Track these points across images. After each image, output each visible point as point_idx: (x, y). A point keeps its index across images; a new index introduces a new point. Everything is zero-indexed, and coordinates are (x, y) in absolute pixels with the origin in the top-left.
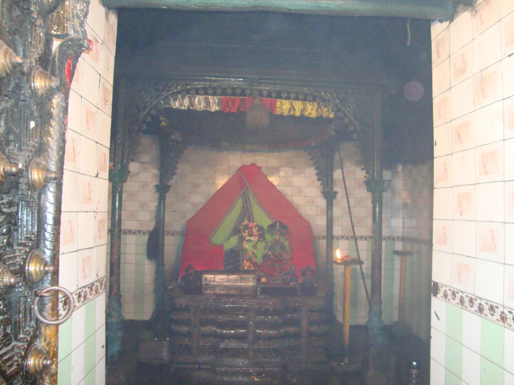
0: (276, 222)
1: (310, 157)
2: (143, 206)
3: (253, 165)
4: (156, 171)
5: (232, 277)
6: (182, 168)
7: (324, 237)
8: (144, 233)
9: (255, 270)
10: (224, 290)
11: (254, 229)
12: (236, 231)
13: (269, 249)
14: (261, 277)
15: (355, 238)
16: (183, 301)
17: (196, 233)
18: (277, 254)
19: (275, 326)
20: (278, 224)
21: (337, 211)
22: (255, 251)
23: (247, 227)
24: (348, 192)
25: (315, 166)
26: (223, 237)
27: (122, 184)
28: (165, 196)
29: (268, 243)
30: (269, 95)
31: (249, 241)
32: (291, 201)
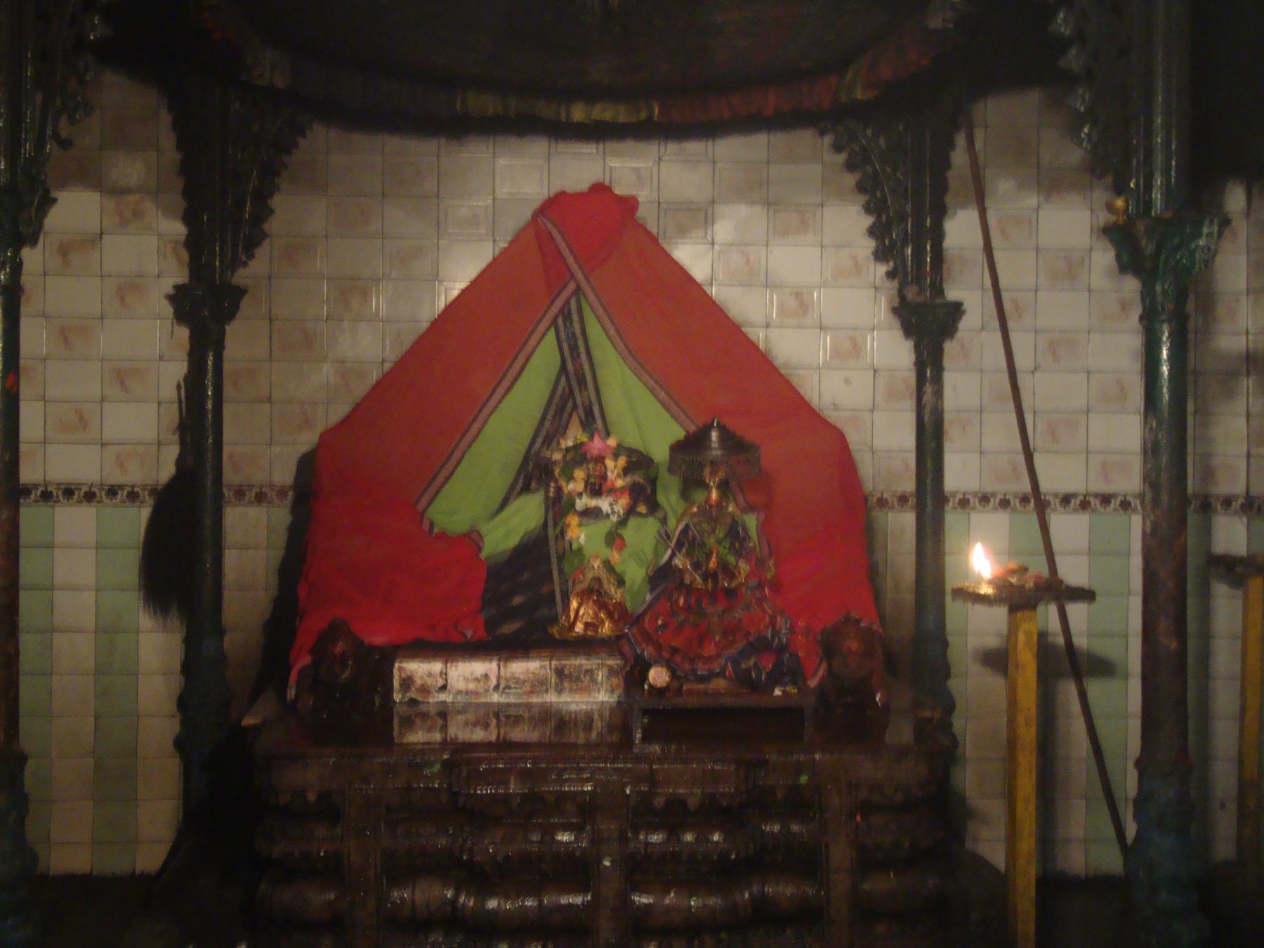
1: (842, 157)
2: (123, 377)
3: (600, 189)
4: (178, 229)
5: (521, 668)
6: (291, 212)
7: (903, 499)
8: (133, 496)
10: (486, 726)
11: (610, 463)
12: (534, 473)
13: (679, 545)
14: (648, 667)
15: (1037, 501)
16: (309, 776)
17: (362, 478)
18: (712, 564)
19: (720, 873)
20: (714, 435)
21: (962, 387)
22: (615, 557)
23: (578, 456)
24: (1008, 306)
25: (863, 199)
26: (479, 504)
27: (17, 252)
31: (591, 514)
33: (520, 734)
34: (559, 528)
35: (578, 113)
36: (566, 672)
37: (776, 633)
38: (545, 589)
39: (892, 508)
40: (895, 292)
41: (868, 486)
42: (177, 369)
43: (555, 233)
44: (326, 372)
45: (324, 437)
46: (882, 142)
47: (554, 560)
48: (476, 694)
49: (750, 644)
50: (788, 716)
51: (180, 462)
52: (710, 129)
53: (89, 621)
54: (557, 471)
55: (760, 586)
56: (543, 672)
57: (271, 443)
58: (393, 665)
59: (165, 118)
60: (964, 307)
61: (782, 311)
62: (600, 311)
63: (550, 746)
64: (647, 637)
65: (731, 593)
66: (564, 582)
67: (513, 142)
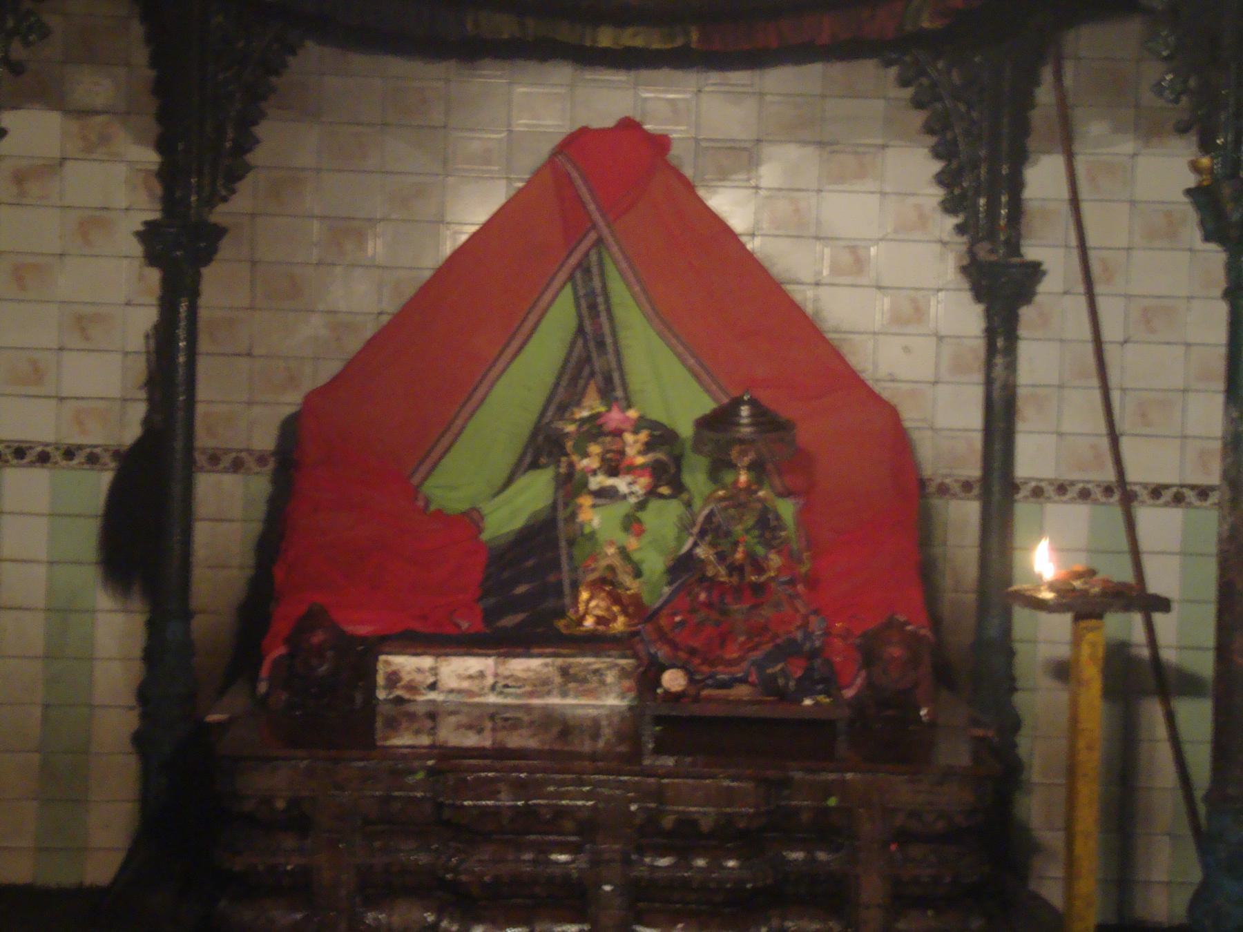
0: (737, 403)
1: (909, 92)
2: (84, 324)
3: (629, 125)
4: (150, 158)
5: (521, 666)
6: (279, 141)
7: (967, 486)
8: (93, 459)
9: (635, 634)
10: (480, 731)
11: (629, 437)
12: (544, 447)
13: (702, 533)
14: (663, 668)
15: (1123, 494)
16: (277, 782)
17: (345, 455)
18: (739, 556)
20: (745, 411)
21: (1039, 360)
22: (632, 543)
23: (594, 429)
26: (482, 481)
28: (197, 279)
29: (698, 503)
32: (809, 309)
33: (515, 741)
34: (569, 510)
35: (605, 38)
36: (572, 671)
37: (808, 636)
38: (552, 578)
39: (954, 496)
40: (964, 248)
41: (927, 472)
42: (148, 316)
43: (575, 175)
44: (315, 326)
45: (309, 398)
46: (956, 77)
47: (563, 544)
48: (470, 693)
49: (777, 646)
50: (816, 726)
51: (147, 422)
52: (755, 59)
53: (38, 597)
54: (569, 445)
55: (792, 582)
56: (546, 670)
57: (250, 403)
58: (377, 660)
59: (137, 29)
60: (1044, 267)
61: (836, 269)
62: (624, 265)
63: (552, 754)
64: (662, 636)
65: (758, 588)
66: (574, 569)
67: (532, 67)
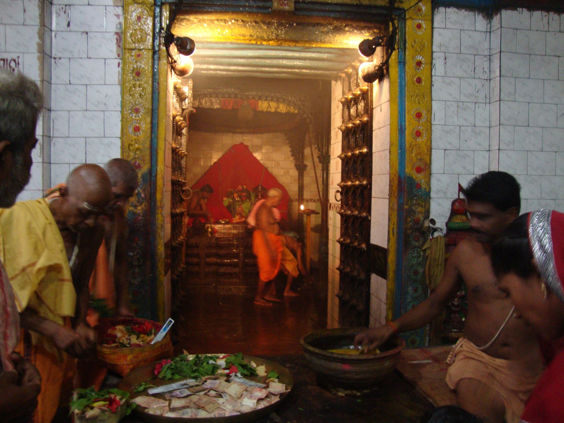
7: (296, 200)
21: (307, 180)
30: (254, 98)
